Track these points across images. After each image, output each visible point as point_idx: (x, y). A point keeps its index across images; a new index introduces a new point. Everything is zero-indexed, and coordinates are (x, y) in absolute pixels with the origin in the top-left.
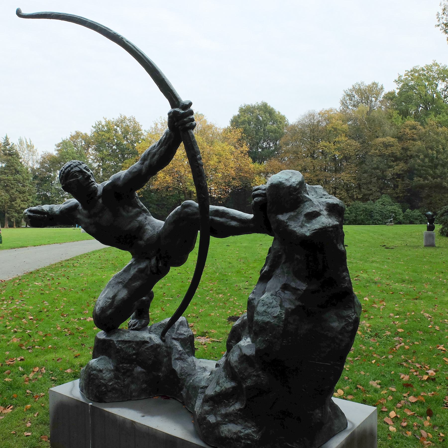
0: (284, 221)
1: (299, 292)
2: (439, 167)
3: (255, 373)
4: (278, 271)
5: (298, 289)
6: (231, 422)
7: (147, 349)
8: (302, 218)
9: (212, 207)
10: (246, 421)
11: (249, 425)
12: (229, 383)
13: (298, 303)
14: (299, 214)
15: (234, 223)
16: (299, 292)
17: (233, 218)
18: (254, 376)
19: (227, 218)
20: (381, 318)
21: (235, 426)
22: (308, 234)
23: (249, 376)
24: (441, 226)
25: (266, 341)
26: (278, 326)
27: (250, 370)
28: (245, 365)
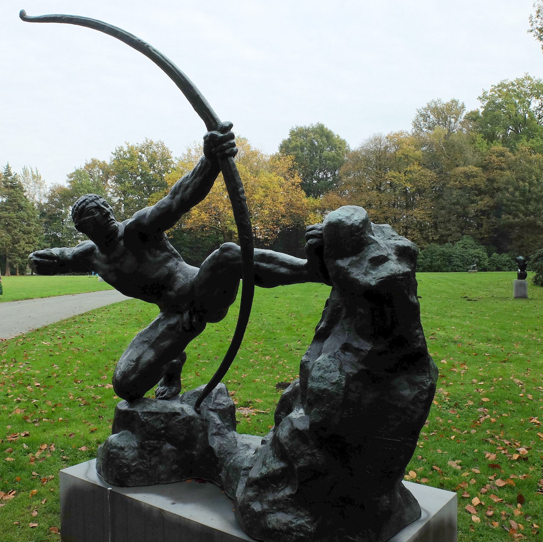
0: (344, 268)
4: (337, 328)
5: (362, 350)
7: (178, 422)
9: (257, 251)
10: (298, 509)
11: (302, 514)
13: (361, 367)
14: (362, 259)
15: (283, 270)
16: (363, 353)
17: (283, 264)
18: (308, 454)
19: (275, 264)
21: (284, 515)
22: (373, 283)
23: (302, 455)
25: (323, 412)
26: (338, 395)
27: (303, 448)
28: (297, 441)
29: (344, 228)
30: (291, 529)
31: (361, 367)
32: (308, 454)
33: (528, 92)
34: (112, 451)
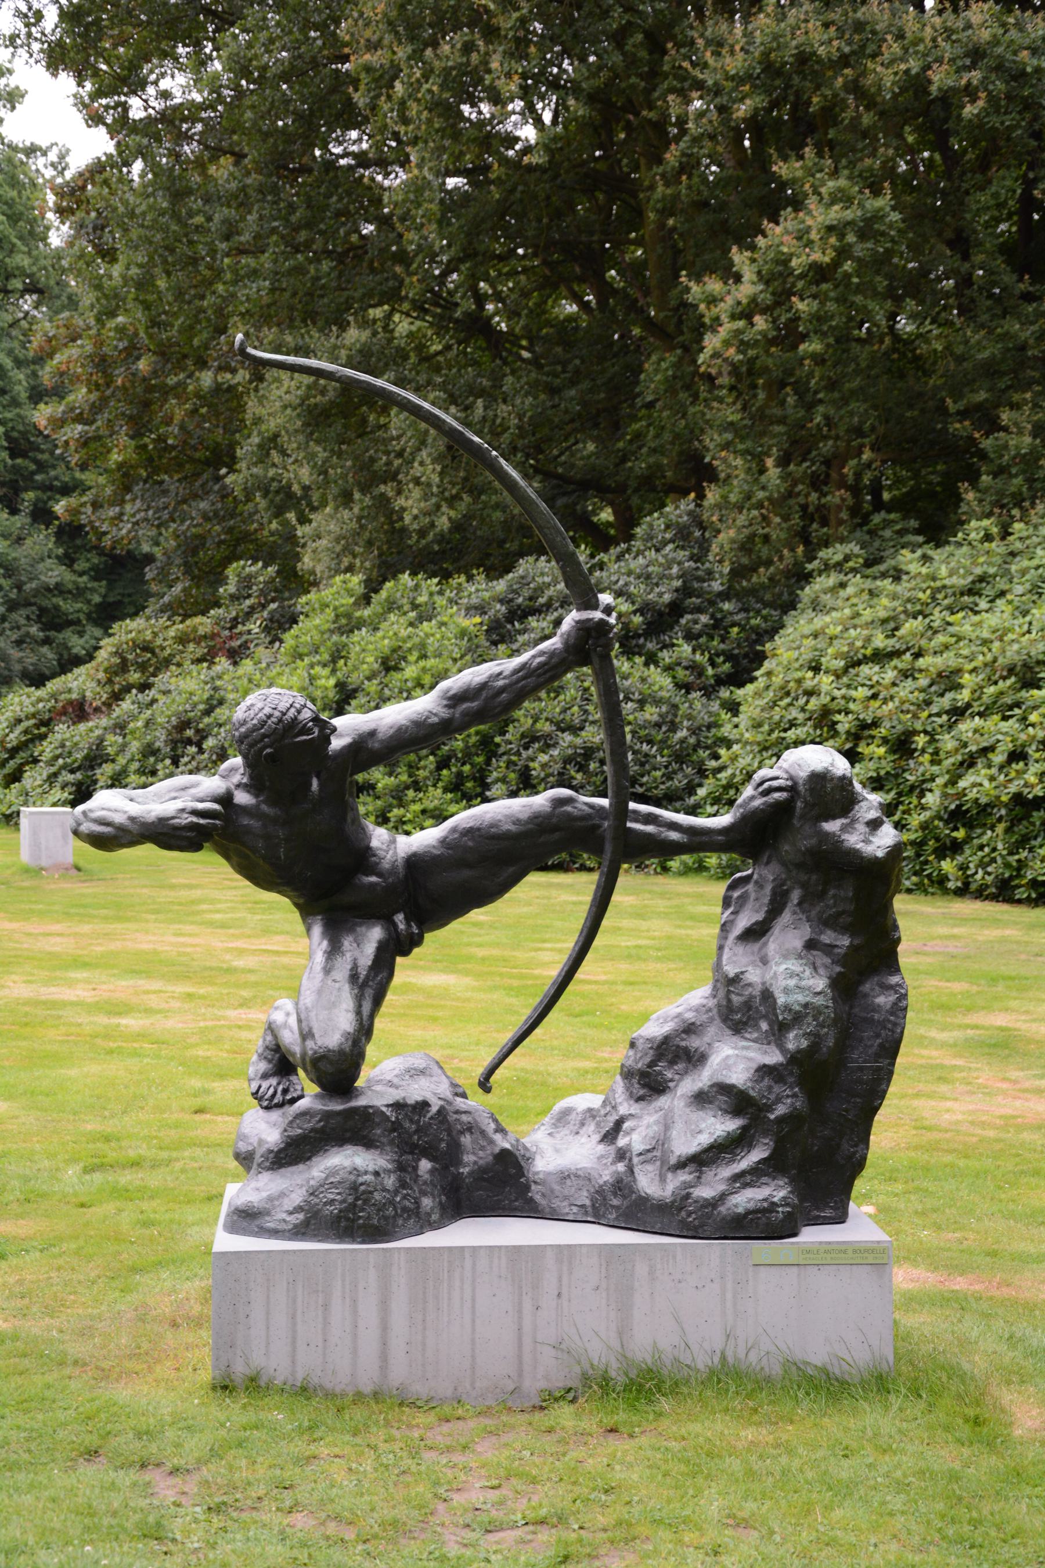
0: (834, 834)
1: (837, 951)
2: (802, 413)
3: (788, 1092)
4: (786, 917)
5: (836, 946)
6: (745, 1185)
7: (431, 1118)
8: (861, 828)
9: (632, 805)
10: (774, 1179)
11: (781, 1183)
12: (728, 1123)
13: (838, 969)
14: (854, 821)
15: (674, 836)
16: (837, 951)
17: (674, 826)
18: (788, 1096)
19: (659, 826)
20: (189, 1202)
21: (756, 1190)
22: (880, 854)
23: (779, 1100)
24: (611, 519)
25: (809, 1034)
26: (827, 1007)
27: (777, 1089)
28: (766, 1081)
29: (832, 779)
30: (773, 1204)
31: (838, 969)
32: (788, 1096)
33: (17, 388)
34: (361, 1180)
